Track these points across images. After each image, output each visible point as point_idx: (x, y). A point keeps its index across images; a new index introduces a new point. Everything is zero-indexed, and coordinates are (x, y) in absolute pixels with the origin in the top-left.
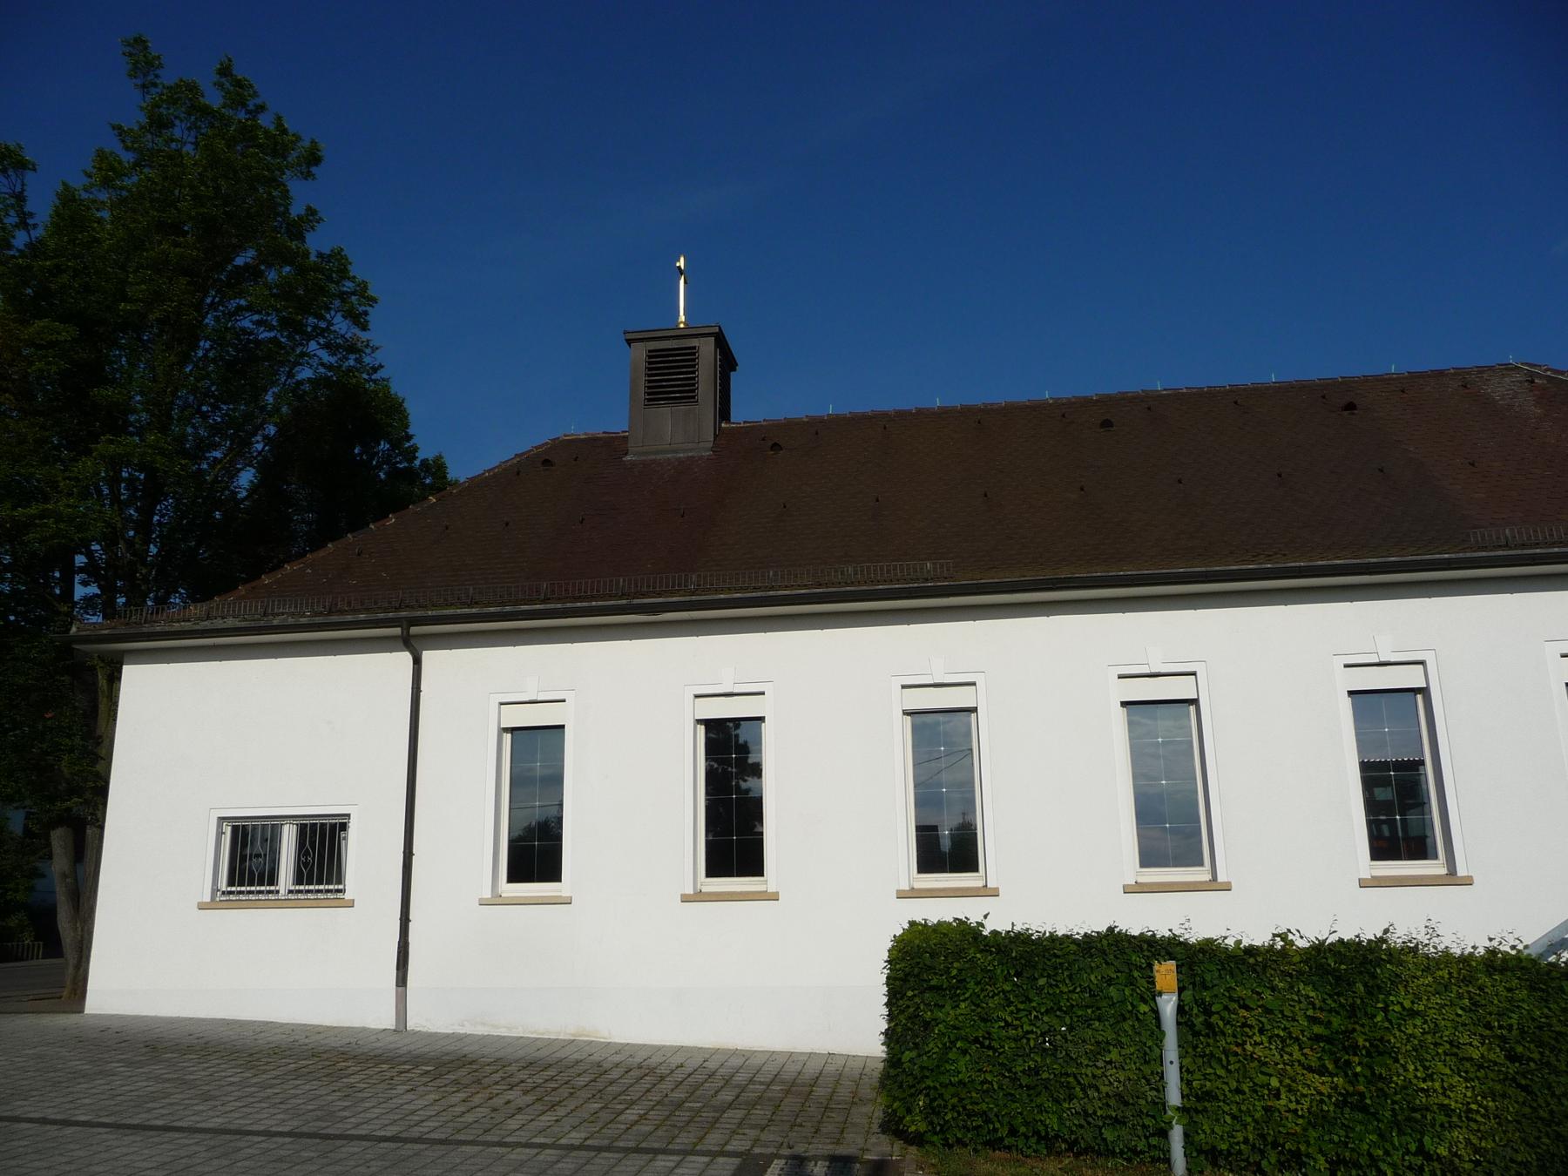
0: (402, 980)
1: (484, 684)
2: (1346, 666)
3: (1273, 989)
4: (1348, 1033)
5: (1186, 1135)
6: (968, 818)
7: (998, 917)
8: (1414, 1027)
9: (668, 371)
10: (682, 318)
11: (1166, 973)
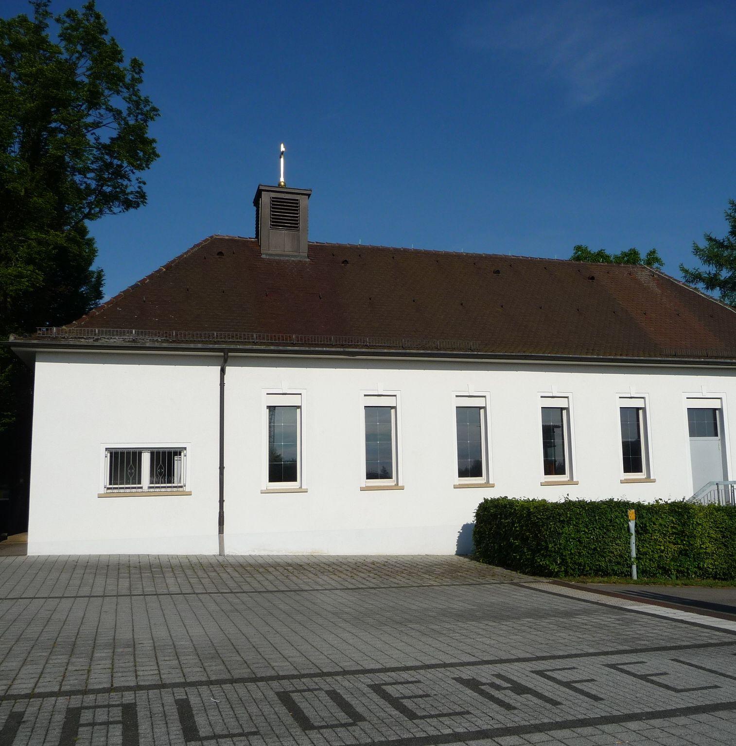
0: (221, 531)
1: (257, 385)
2: (542, 397)
3: (662, 518)
4: (683, 532)
5: (637, 567)
6: (294, 459)
7: (576, 494)
8: (699, 528)
9: (285, 211)
10: (282, 179)
11: (632, 513)
